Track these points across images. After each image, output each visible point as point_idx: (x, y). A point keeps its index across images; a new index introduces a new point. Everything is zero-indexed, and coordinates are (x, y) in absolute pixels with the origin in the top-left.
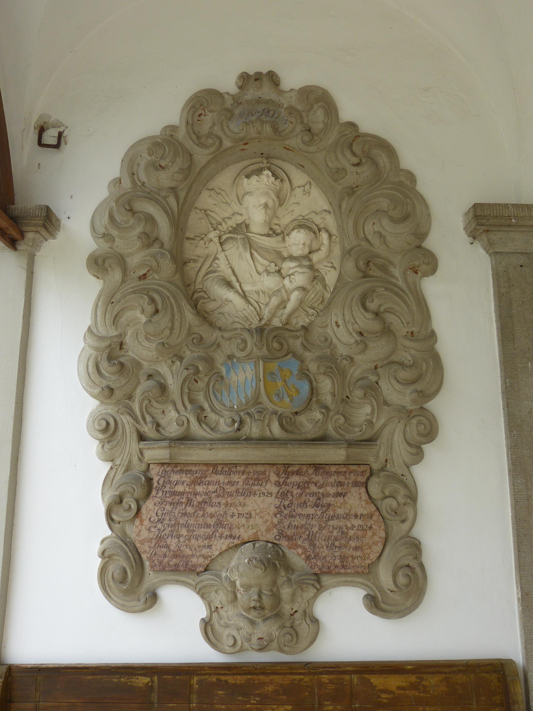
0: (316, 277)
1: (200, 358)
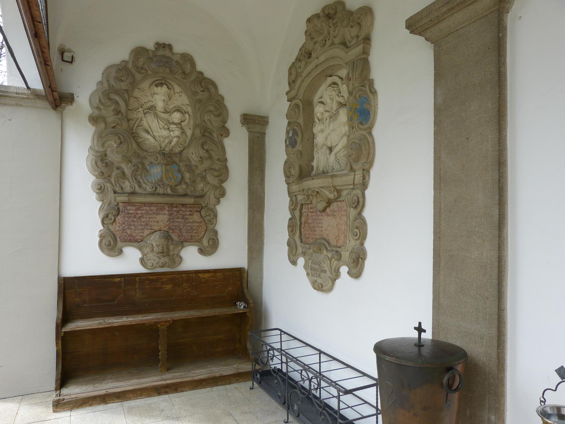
0: (183, 132)
1: (139, 163)
